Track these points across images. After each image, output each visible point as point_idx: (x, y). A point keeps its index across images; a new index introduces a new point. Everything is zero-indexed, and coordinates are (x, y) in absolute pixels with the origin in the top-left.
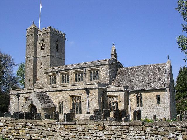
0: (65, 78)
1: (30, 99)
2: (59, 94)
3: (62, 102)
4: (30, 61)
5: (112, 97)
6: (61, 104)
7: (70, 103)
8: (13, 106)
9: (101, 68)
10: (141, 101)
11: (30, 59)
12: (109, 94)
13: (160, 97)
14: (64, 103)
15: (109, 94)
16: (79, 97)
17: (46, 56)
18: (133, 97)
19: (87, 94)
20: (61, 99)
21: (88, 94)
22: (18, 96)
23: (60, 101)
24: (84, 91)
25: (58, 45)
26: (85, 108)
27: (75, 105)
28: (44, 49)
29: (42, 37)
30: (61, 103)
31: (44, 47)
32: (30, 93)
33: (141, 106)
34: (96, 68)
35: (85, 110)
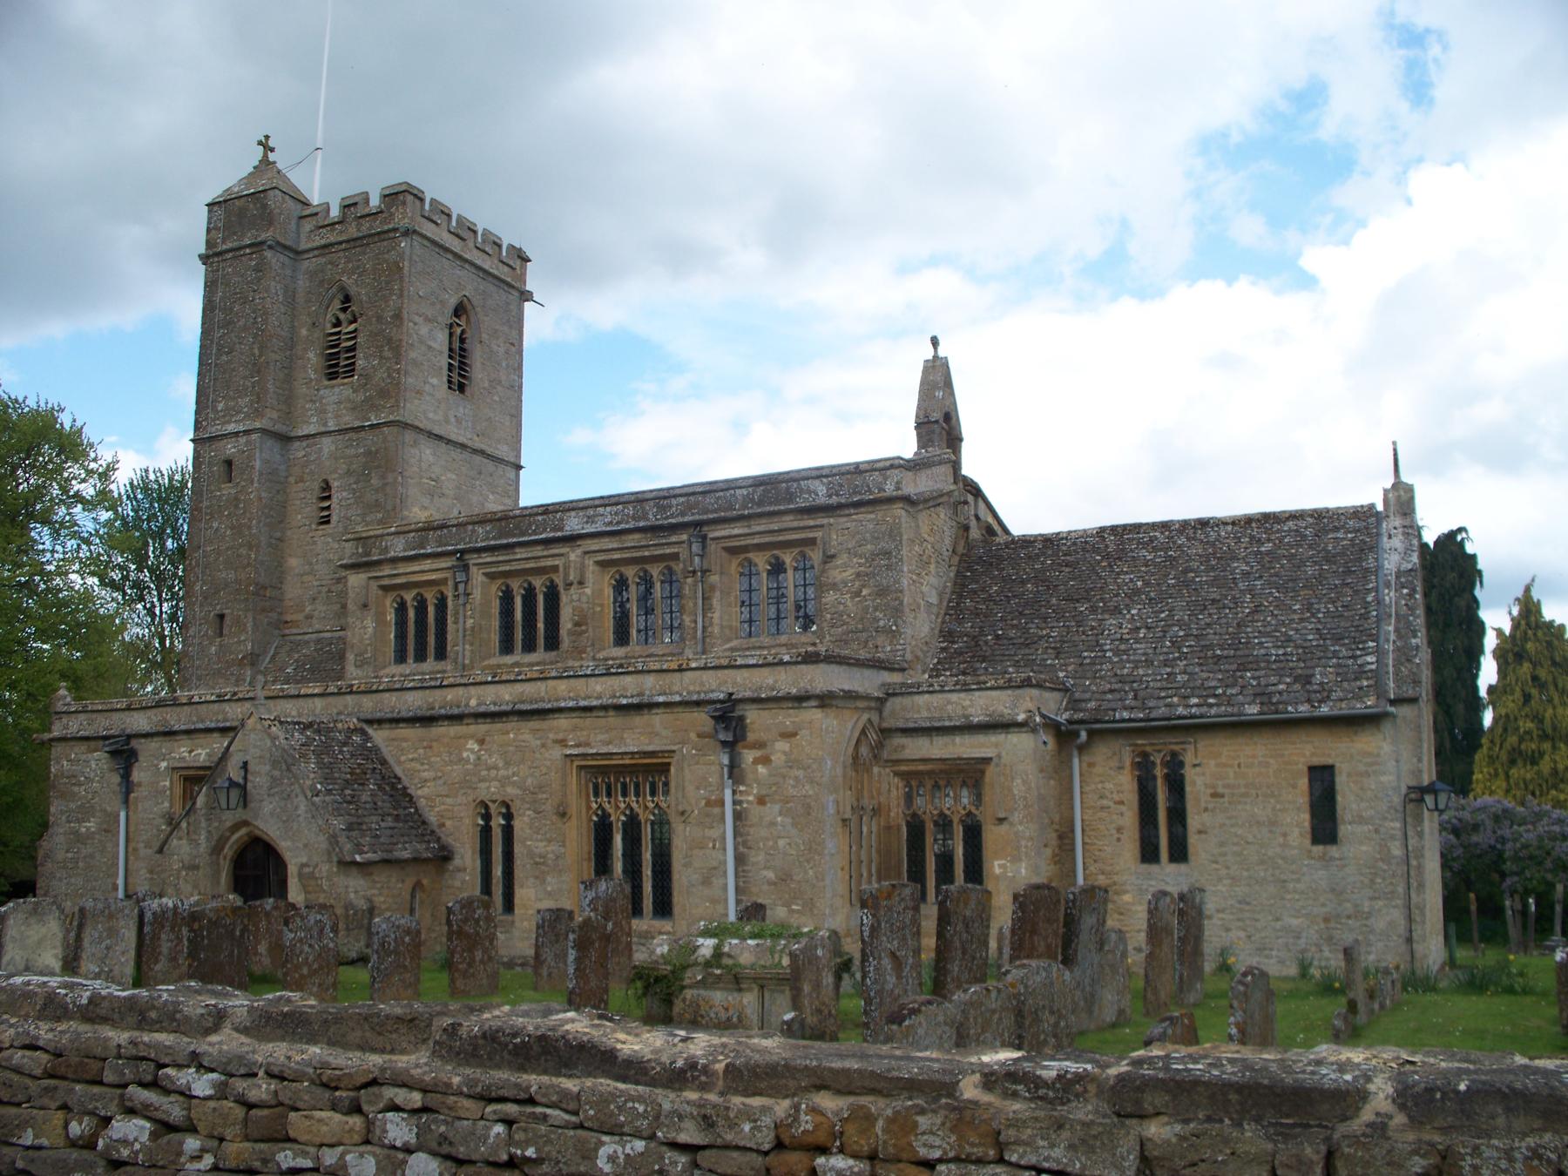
2: (476, 747)
3: (509, 816)
6: (497, 833)
8: (79, 838)
10: (1178, 815)
13: (1341, 781)
20: (490, 790)
21: (731, 746)
22: (123, 753)
23: (487, 807)
24: (949, 465)
25: (462, 340)
27: (618, 840)
28: (351, 370)
30: (498, 822)
31: (352, 349)
32: (224, 731)
33: (1179, 853)
35: (706, 882)
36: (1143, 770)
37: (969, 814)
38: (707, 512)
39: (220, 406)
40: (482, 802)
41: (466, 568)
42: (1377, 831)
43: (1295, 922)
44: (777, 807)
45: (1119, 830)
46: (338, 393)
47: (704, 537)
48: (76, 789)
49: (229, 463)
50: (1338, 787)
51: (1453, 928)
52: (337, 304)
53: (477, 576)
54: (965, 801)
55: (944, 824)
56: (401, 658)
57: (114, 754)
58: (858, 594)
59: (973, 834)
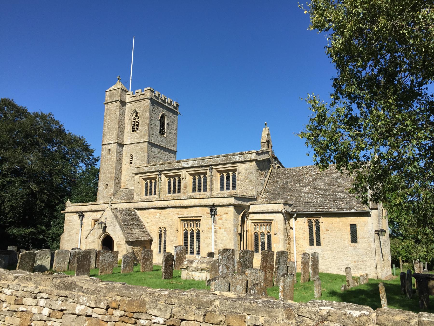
0: (175, 187)
1: (102, 223)
2: (159, 215)
3: (165, 231)
4: (110, 150)
5: (260, 223)
7: (179, 232)
9: (241, 168)
11: (110, 147)
12: (245, 249)
13: (358, 228)
14: (167, 233)
15: (245, 249)
16: (196, 220)
17: (140, 143)
18: (300, 226)
19: (212, 215)
22: (81, 215)
26: (207, 245)
28: (137, 130)
29: (135, 106)
31: (138, 125)
33: (319, 244)
34: (231, 167)
35: (208, 247)
36: (310, 223)
37: (268, 232)
38: (213, 163)
39: (108, 137)
40: (160, 228)
41: (161, 175)
42: (367, 241)
43: (347, 262)
44: (223, 230)
45: (304, 237)
46: (136, 134)
47: (212, 168)
48: (70, 224)
49: (110, 150)
50: (357, 230)
51: (394, 266)
52: (135, 115)
53: (163, 176)
54: (268, 229)
55: (263, 234)
56: (146, 194)
57: (80, 216)
58: (245, 181)
59: (269, 237)
